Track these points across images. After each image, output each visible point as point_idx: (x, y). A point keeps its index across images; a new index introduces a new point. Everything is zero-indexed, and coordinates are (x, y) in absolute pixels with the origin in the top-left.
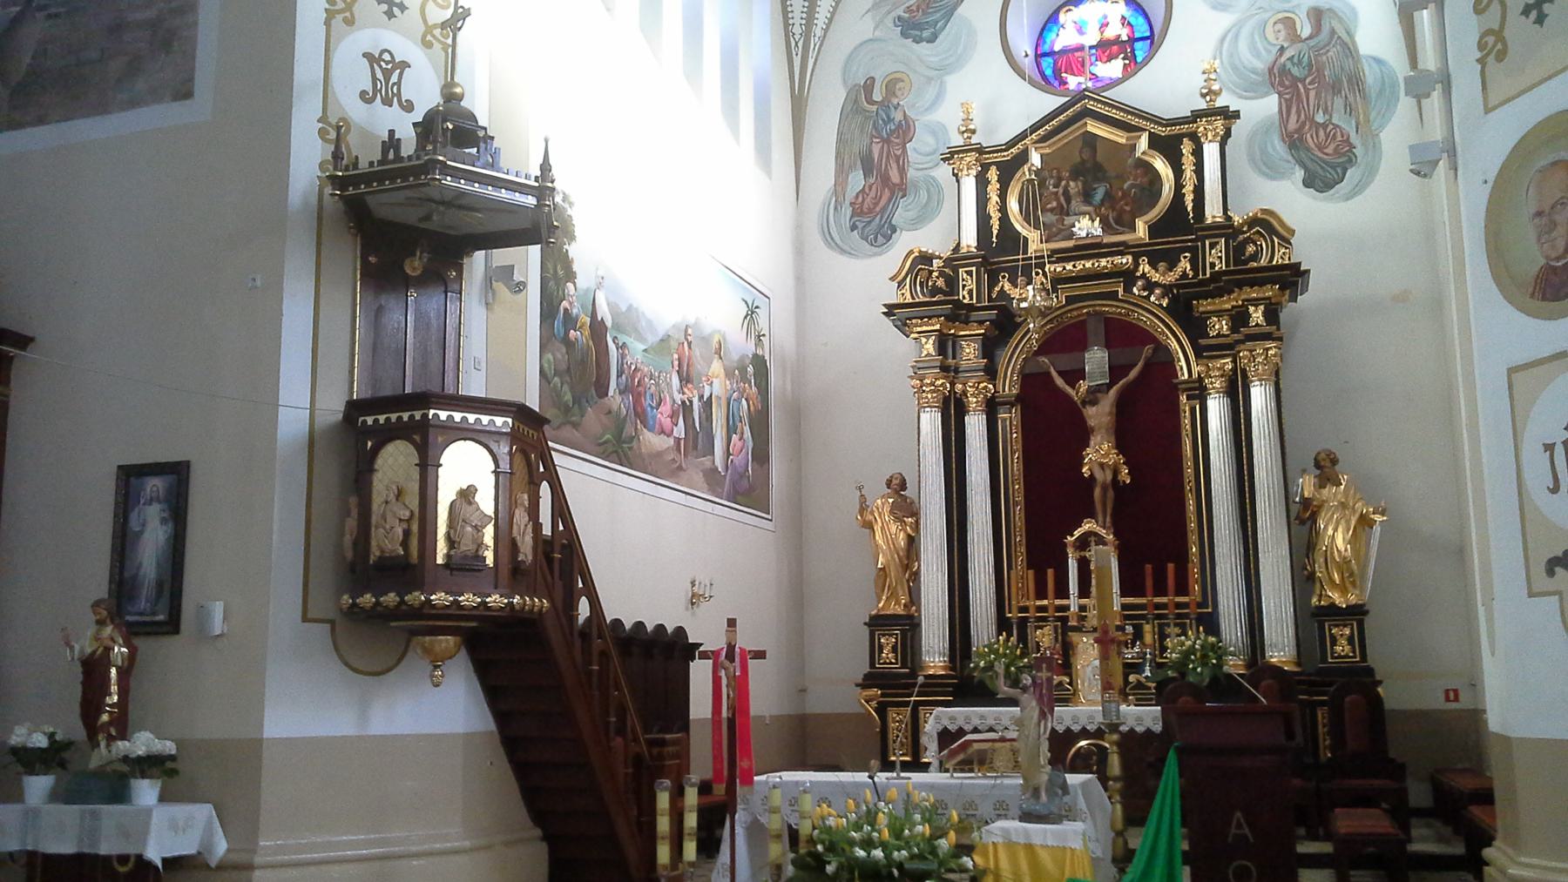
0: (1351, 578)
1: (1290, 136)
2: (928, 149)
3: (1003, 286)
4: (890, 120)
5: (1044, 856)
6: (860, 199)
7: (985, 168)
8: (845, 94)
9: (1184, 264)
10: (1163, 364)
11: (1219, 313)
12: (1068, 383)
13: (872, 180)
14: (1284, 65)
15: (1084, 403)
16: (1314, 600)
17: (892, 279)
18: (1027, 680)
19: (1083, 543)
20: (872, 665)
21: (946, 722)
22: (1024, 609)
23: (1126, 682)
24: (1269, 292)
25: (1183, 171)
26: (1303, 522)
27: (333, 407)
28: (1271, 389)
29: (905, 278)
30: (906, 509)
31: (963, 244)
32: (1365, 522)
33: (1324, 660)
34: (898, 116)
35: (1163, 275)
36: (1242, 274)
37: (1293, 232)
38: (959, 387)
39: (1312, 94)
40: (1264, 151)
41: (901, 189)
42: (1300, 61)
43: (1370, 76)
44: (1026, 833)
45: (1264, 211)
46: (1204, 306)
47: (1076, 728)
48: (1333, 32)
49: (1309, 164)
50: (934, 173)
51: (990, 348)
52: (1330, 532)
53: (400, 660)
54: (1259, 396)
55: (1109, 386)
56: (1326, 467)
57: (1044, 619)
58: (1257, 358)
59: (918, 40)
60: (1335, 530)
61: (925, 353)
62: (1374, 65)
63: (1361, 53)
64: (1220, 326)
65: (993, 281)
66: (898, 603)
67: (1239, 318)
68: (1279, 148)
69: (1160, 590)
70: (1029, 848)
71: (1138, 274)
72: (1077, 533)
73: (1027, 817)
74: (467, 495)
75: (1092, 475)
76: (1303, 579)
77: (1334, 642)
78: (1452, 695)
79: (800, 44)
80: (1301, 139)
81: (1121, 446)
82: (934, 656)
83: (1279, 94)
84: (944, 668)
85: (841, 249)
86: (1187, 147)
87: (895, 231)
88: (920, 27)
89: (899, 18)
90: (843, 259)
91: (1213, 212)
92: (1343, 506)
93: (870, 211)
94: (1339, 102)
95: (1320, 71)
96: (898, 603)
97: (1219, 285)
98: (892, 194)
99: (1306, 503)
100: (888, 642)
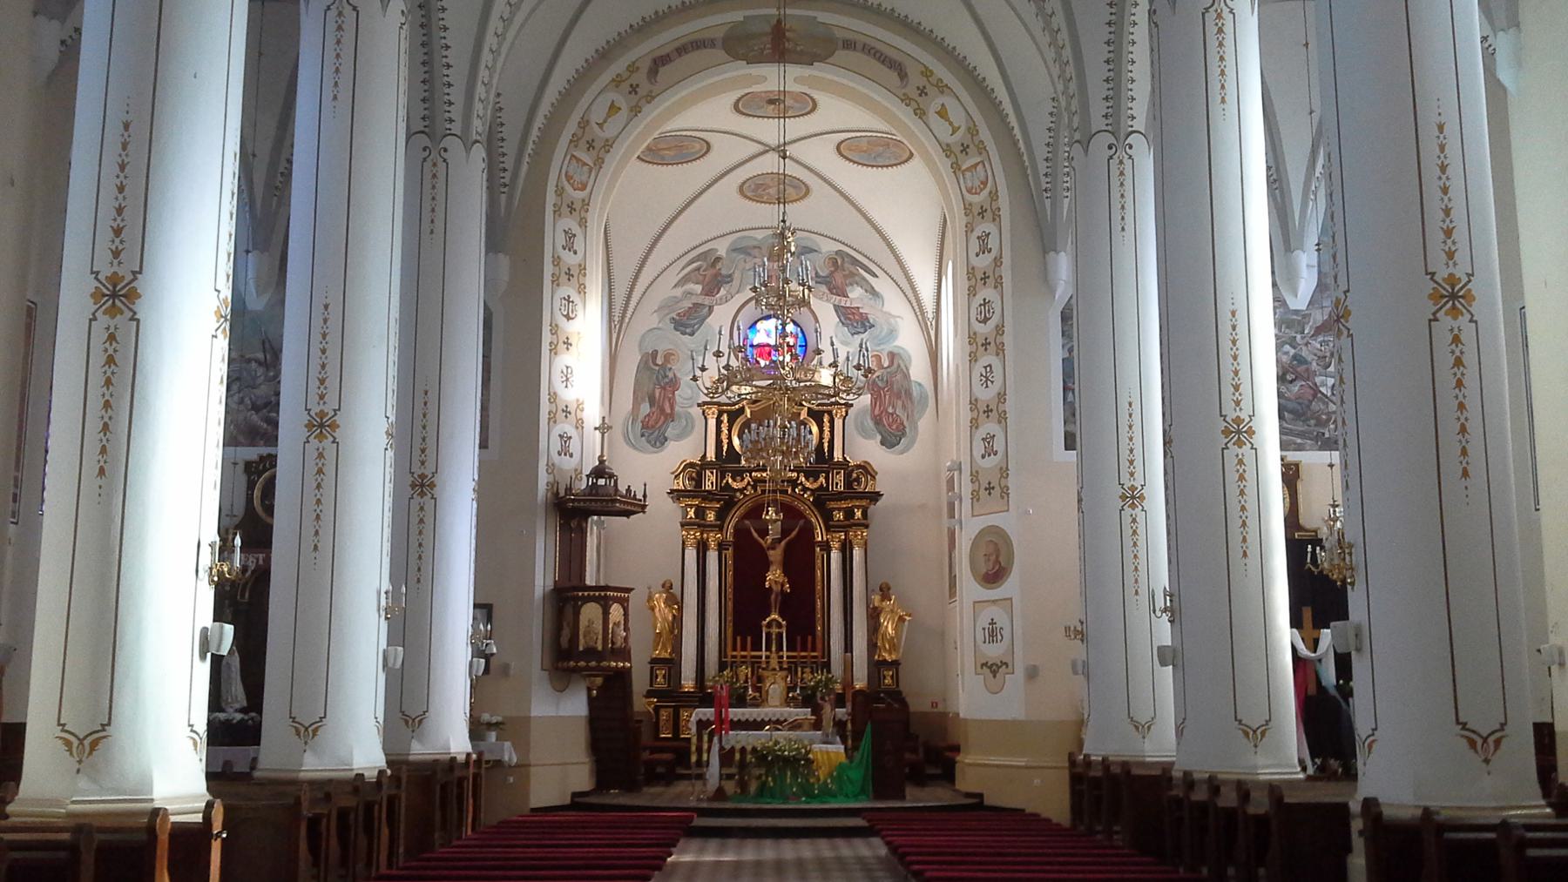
0: (894, 647)
1: (875, 417)
2: (686, 396)
3: (727, 481)
4: (666, 376)
5: (832, 755)
6: (647, 420)
7: (720, 414)
8: (639, 358)
9: (822, 480)
10: (808, 530)
11: (839, 509)
12: (760, 536)
13: (654, 409)
14: (875, 380)
15: (768, 549)
16: (876, 657)
17: (673, 473)
18: (827, 698)
19: (769, 625)
20: (651, 686)
21: (701, 716)
22: (733, 657)
23: (788, 697)
24: (864, 503)
25: (823, 431)
26: (873, 618)
27: (550, 584)
28: (863, 551)
29: (680, 474)
30: (675, 601)
31: (708, 455)
32: (901, 619)
33: (880, 686)
34: (670, 375)
35: (811, 484)
36: (850, 492)
37: (876, 473)
38: (705, 535)
39: (887, 397)
40: (862, 423)
41: (671, 417)
42: (882, 379)
43: (915, 392)
44: (827, 748)
45: (866, 462)
46: (833, 505)
47: (767, 719)
48: (899, 366)
49: (883, 433)
50: (690, 410)
51: (722, 515)
52: (886, 623)
53: (567, 687)
54: (857, 553)
55: (780, 540)
56: (885, 592)
57: (743, 662)
58: (858, 536)
59: (684, 333)
60: (888, 623)
61: (689, 517)
62: (918, 387)
63: (912, 378)
64: (839, 516)
65: (723, 477)
66: (666, 651)
67: (849, 513)
68: (870, 423)
69: (804, 650)
70: (828, 752)
71: (799, 482)
72: (768, 620)
73: (825, 743)
74: (591, 622)
75: (770, 587)
76: (872, 646)
77: (885, 678)
78: (935, 705)
79: (617, 327)
80: (881, 419)
81: (786, 572)
82: (688, 683)
83: (872, 395)
84: (693, 688)
85: (634, 446)
86: (826, 419)
87: (666, 440)
88: (686, 326)
89: (673, 318)
90: (636, 452)
91: (838, 456)
92: (892, 611)
93: (653, 427)
94: (900, 403)
95: (892, 385)
96: (666, 651)
97: (839, 496)
98: (666, 419)
99: (875, 608)
100: (660, 673)
